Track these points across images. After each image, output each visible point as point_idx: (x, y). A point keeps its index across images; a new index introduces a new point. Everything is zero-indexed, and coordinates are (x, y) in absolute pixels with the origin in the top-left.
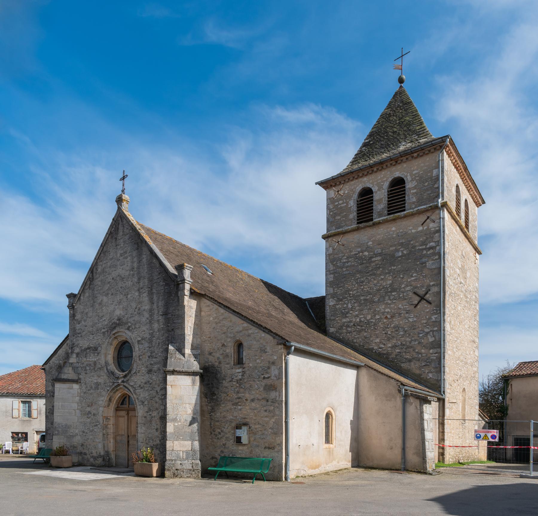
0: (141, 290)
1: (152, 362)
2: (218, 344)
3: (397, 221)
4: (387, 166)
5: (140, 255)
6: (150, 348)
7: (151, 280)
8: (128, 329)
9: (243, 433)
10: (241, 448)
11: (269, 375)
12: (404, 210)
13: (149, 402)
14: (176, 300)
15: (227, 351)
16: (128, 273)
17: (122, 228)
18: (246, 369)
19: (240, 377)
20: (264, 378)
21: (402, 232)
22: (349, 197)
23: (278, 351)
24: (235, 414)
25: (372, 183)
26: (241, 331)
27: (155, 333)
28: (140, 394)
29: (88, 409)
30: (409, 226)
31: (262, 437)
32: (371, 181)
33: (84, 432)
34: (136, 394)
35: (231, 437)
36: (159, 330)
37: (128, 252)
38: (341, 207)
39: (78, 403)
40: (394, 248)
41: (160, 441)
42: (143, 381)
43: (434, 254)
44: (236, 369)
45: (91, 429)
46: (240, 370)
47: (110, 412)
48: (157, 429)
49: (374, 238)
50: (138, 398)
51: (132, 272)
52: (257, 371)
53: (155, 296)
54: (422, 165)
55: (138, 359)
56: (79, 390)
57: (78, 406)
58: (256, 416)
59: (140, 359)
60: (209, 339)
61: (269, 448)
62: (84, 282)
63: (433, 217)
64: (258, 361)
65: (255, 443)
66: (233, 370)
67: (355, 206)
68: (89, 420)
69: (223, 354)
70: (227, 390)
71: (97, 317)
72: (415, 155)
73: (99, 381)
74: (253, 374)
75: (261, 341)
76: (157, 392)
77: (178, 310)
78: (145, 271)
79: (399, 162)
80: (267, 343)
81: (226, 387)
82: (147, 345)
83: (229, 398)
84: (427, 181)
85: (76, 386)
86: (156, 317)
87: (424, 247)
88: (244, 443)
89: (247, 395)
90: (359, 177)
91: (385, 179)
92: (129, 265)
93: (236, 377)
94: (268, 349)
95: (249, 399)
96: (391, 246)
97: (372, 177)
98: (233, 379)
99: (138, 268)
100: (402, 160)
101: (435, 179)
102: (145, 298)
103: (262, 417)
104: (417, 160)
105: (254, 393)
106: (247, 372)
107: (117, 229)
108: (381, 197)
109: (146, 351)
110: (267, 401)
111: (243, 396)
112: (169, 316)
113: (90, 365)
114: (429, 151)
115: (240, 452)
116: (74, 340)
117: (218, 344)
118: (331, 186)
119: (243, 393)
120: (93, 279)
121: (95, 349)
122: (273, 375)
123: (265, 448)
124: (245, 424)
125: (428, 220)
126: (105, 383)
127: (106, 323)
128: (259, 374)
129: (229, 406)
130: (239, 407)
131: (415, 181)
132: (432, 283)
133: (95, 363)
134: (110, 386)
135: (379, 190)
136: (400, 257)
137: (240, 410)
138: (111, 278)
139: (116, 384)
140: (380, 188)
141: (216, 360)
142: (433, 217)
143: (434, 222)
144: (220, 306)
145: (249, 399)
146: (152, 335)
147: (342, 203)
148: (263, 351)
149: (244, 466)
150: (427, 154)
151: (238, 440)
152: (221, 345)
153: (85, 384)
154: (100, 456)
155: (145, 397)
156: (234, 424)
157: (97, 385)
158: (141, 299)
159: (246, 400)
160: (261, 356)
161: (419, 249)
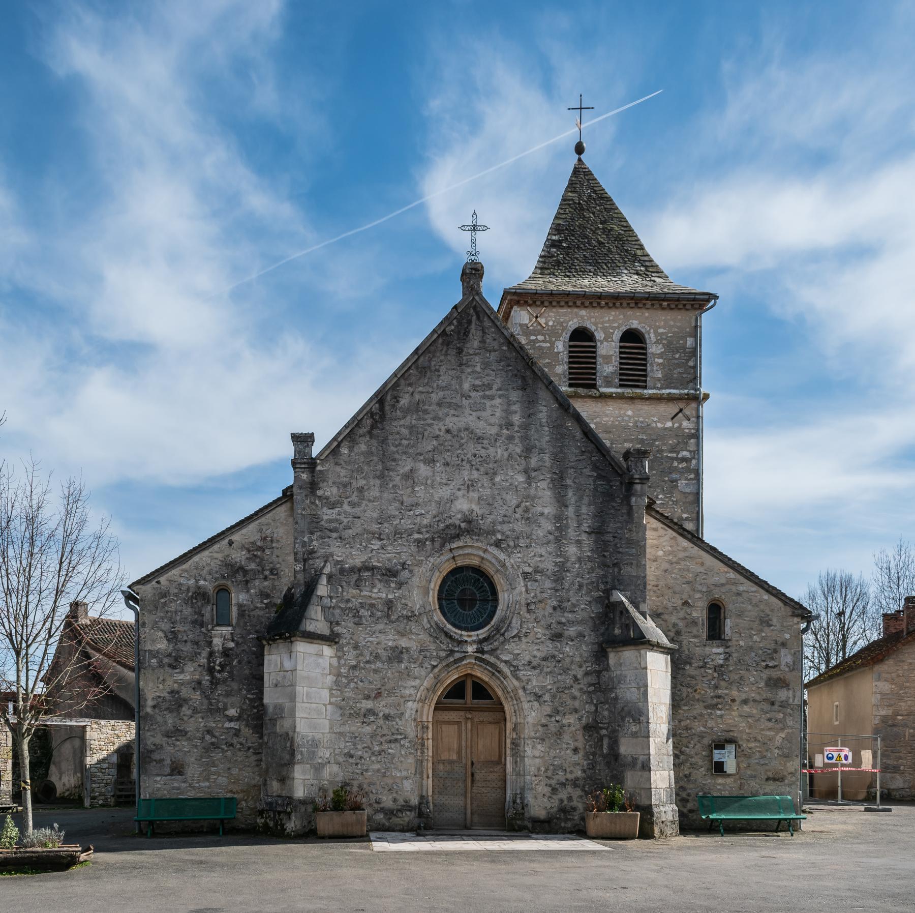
0: (533, 474)
1: (564, 620)
2: (673, 601)
3: (636, 401)
4: (621, 304)
5: (530, 403)
6: (557, 590)
7: (559, 458)
8: (497, 544)
9: (728, 758)
10: (720, 781)
12: (645, 387)
13: (554, 697)
14: (624, 511)
15: (695, 614)
16: (494, 430)
17: (480, 333)
18: (733, 649)
19: (721, 662)
20: (767, 666)
21: (642, 422)
22: (553, 334)
23: (792, 626)
24: (710, 723)
25: (595, 324)
26: (723, 585)
27: (569, 564)
28: (529, 680)
29: (369, 704)
30: (653, 416)
31: (762, 762)
32: (593, 320)
33: (352, 756)
34: (518, 678)
35: (700, 763)
36: (580, 560)
37: (495, 387)
38: (541, 348)
39: (331, 689)
41: (584, 771)
42: (538, 654)
43: (688, 470)
44: (713, 647)
45: (377, 748)
46: (721, 650)
47: (428, 714)
48: (576, 750)
49: (598, 420)
50: (524, 688)
51: (505, 431)
52: (753, 654)
53: (570, 494)
54: (672, 323)
55: (524, 609)
56: (335, 661)
57: (331, 695)
58: (750, 727)
59: (529, 611)
60: (655, 588)
61: (775, 780)
62: (354, 417)
63: (687, 412)
65: (749, 772)
66: (707, 649)
68: (368, 729)
69: (686, 618)
70: (694, 682)
71: (397, 504)
72: (665, 304)
73: (403, 643)
74: (747, 658)
75: (762, 607)
76: (576, 679)
77: (630, 530)
78: (544, 437)
79: (640, 305)
80: (772, 610)
81: (692, 677)
82: (548, 584)
83: (697, 697)
84: (678, 352)
85: (328, 651)
86: (572, 533)
87: (675, 455)
88: (729, 772)
89: (735, 693)
90: (575, 305)
91: (616, 325)
92: (498, 414)
93: (713, 660)
94: (775, 621)
95: (738, 700)
96: (626, 441)
97: (597, 313)
98: (706, 663)
99: (525, 427)
100: (644, 304)
101: (690, 352)
102: (543, 490)
103: (763, 730)
104: (665, 312)
105: (747, 689)
106: (734, 655)
107: (463, 333)
108: (608, 350)
109: (545, 595)
110: (773, 704)
111: (727, 694)
112: (609, 537)
113: (372, 606)
114: (685, 305)
115: (719, 787)
116: (315, 543)
117: (673, 601)
118: (526, 302)
119: (726, 688)
120: (383, 417)
121: (390, 574)
122: (783, 663)
123: (767, 779)
124: (731, 741)
125: (680, 415)
126: (421, 651)
127: (425, 522)
128: (757, 659)
129: (698, 709)
130: (719, 712)
131: (661, 346)
132: (685, 516)
133: (389, 604)
134: (441, 659)
135: (606, 339)
137: (721, 716)
138: (443, 429)
139: (457, 655)
141: (670, 627)
143: (689, 420)
144: (681, 535)
145: (738, 700)
146: (562, 567)
147: (543, 341)
148: (765, 622)
149: (741, 811)
150: (680, 309)
151: (719, 768)
152: (680, 602)
153: (356, 647)
154: (407, 807)
155: (543, 687)
156: (706, 741)
157: (397, 655)
158: (532, 492)
159: (733, 700)
160: (762, 631)
161: (667, 456)
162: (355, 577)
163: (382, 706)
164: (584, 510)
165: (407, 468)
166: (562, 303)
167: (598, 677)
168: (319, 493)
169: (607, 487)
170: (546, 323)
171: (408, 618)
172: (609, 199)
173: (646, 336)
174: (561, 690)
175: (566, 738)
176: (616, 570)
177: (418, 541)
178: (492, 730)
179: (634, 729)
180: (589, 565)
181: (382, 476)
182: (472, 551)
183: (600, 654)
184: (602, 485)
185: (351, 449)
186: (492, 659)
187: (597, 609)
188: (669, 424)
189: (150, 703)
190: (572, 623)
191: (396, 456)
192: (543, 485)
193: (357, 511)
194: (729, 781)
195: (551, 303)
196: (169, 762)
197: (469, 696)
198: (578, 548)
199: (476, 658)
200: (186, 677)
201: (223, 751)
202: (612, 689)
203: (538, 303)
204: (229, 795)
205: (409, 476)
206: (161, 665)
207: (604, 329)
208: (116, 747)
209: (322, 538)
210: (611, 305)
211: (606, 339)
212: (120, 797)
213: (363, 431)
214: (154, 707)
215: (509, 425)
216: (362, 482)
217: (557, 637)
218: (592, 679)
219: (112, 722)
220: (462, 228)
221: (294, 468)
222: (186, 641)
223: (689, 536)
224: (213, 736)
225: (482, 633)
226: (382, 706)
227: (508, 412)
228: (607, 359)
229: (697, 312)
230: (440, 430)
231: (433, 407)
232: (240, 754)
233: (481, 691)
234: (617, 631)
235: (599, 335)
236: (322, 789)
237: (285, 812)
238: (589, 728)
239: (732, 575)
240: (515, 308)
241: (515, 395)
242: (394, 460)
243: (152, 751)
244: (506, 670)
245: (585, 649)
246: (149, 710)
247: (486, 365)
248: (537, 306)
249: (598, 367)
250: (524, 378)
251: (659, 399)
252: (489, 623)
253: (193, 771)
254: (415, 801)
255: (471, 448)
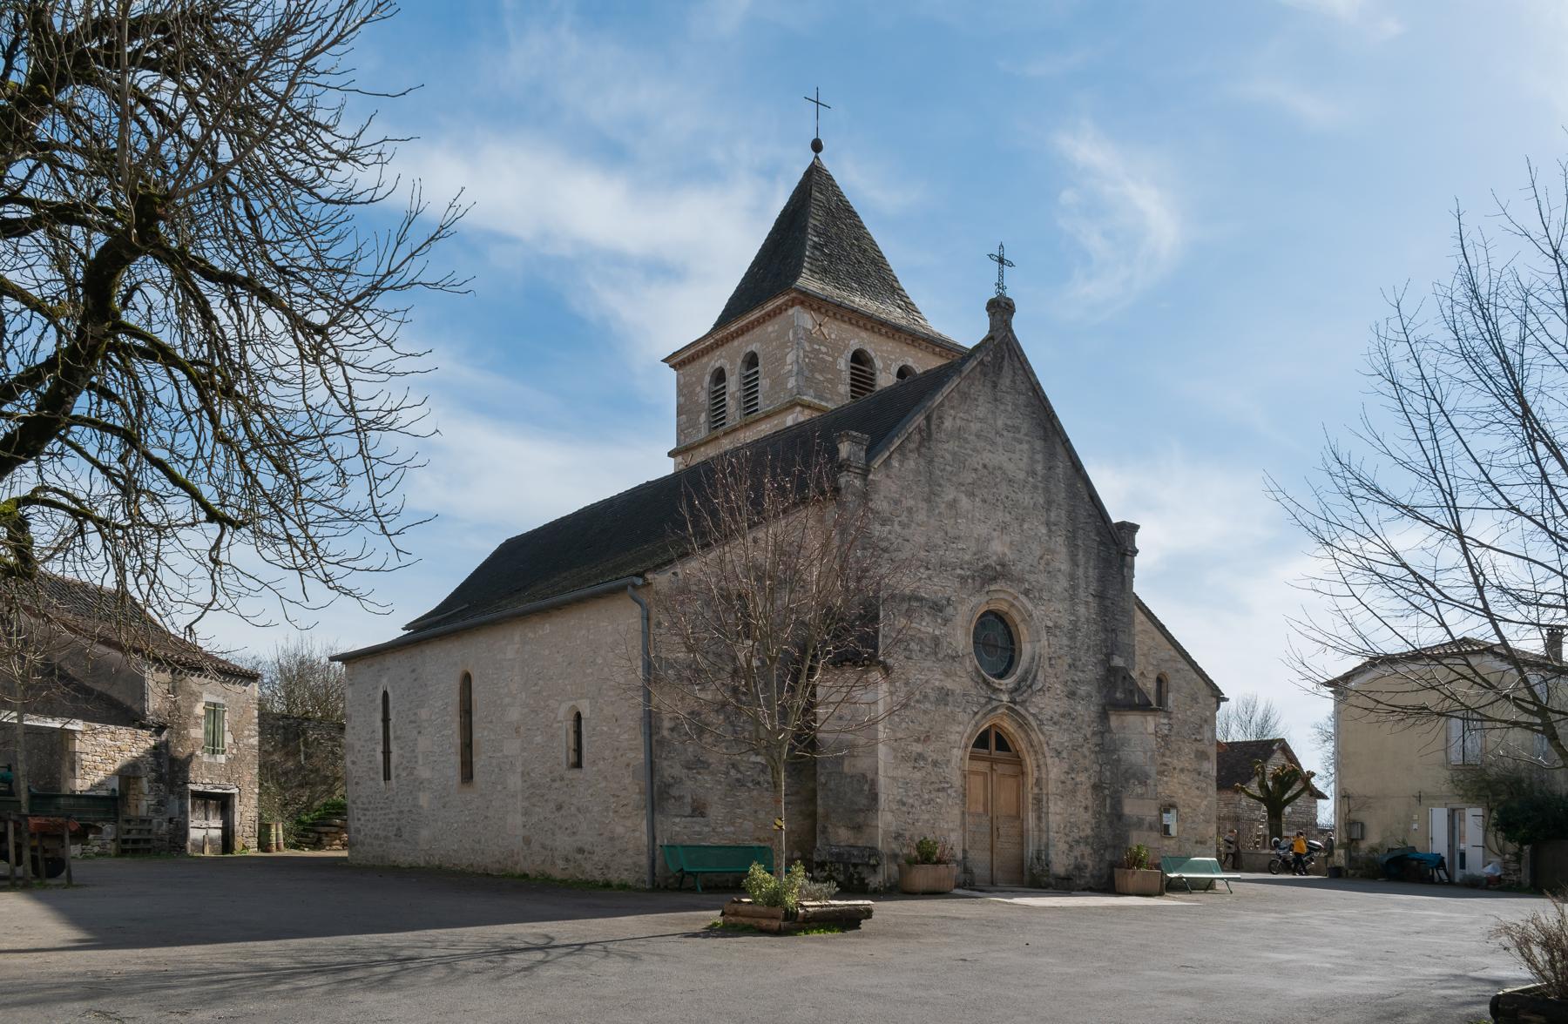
7: (1072, 516)
8: (1026, 593)
9: (1170, 819)
10: (1166, 842)
29: (917, 748)
37: (1023, 431)
38: (824, 361)
48: (1086, 808)
59: (1051, 665)
68: (918, 775)
73: (949, 684)
76: (1086, 739)
86: (1081, 593)
97: (876, 339)
102: (1060, 544)
112: (1108, 603)
113: (921, 640)
121: (937, 608)
127: (967, 558)
133: (936, 640)
139: (995, 704)
146: (1074, 623)
148: (1195, 699)
157: (944, 696)
162: (905, 606)
163: (929, 750)
164: (1091, 572)
165: (951, 497)
171: (953, 658)
172: (855, 215)
174: (1075, 748)
175: (1079, 796)
177: (961, 577)
178: (1011, 782)
179: (1139, 790)
180: (1094, 627)
181: (928, 500)
182: (1001, 597)
183: (1103, 716)
185: (901, 462)
186: (1022, 711)
187: (1100, 671)
189: (667, 724)
190: (1082, 682)
192: (1060, 540)
193: (906, 532)
194: (1172, 842)
197: (992, 744)
198: (1086, 610)
199: (1009, 708)
200: (708, 696)
201: (750, 790)
202: (1115, 751)
204: (755, 844)
205: (953, 505)
206: (679, 677)
208: (117, 765)
212: (125, 841)
213: (912, 446)
214: (672, 730)
215: (1034, 473)
216: (911, 503)
217: (1072, 695)
218: (1097, 739)
219: (112, 728)
224: (739, 771)
226: (929, 750)
227: (1033, 461)
231: (972, 438)
232: (767, 794)
233: (1002, 744)
234: (1119, 695)
235: (879, 364)
237: (867, 864)
238: (1097, 788)
239: (1173, 652)
241: (1039, 444)
243: (670, 786)
244: (1034, 723)
246: (666, 733)
247: (1016, 407)
250: (1045, 429)
253: (716, 812)
255: (1004, 489)
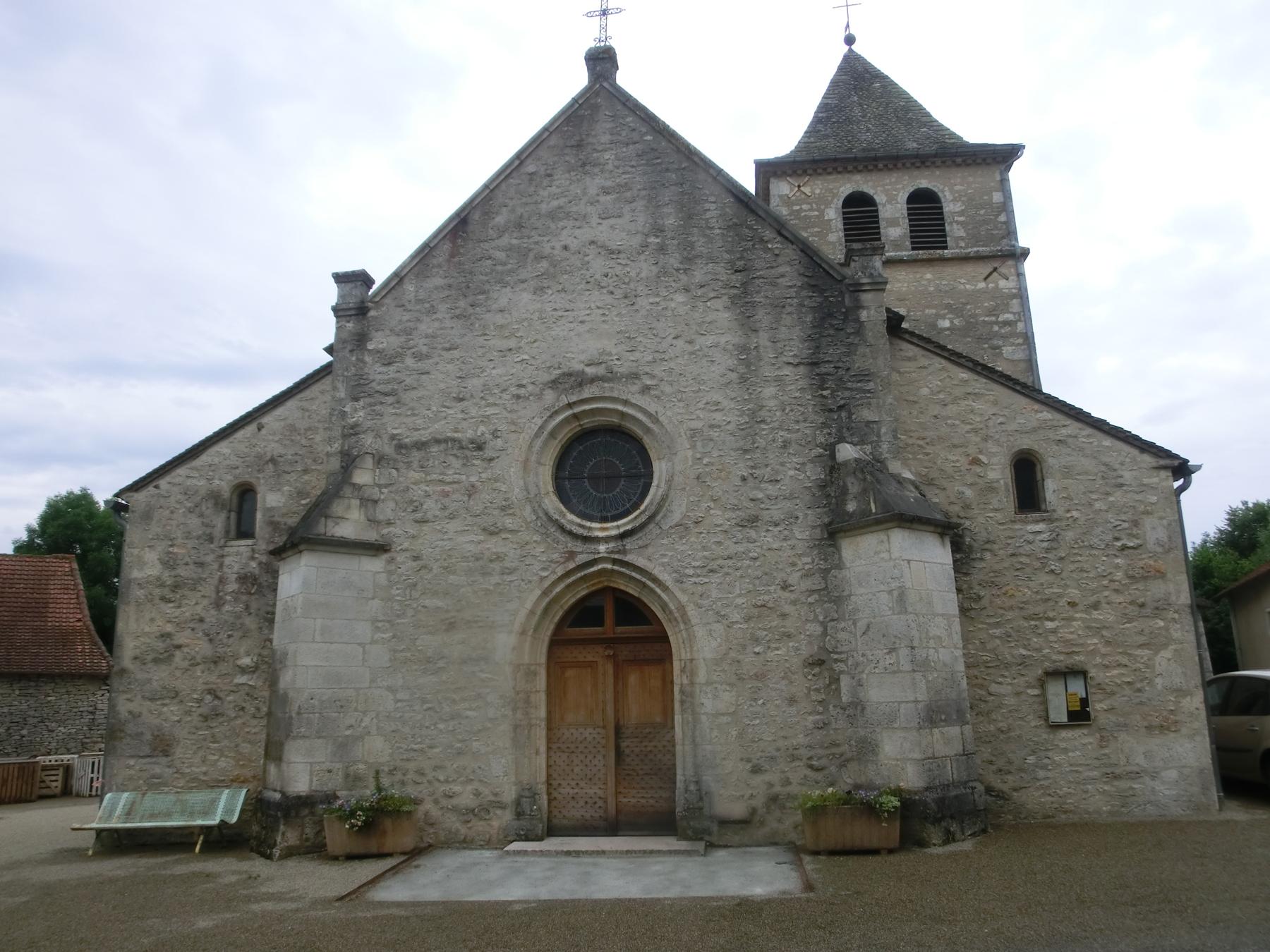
1: (760, 495)
11: (1139, 542)
12: (946, 248)
40: (934, 311)
51: (652, 240)
64: (1097, 505)
67: (840, 219)
85: (374, 565)
96: (928, 307)
111: (1060, 596)
125: (995, 274)
135: (889, 201)
136: (948, 329)
137: (1054, 631)
138: (558, 246)
140: (891, 199)
142: (1003, 270)
166: (830, 170)
167: (824, 578)
168: (370, 346)
169: (819, 300)
170: (813, 193)
173: (940, 195)
176: (844, 414)
184: (811, 297)
187: (815, 473)
188: (982, 285)
191: (487, 287)
195: (815, 170)
196: (148, 737)
203: (800, 172)
207: (886, 192)
209: (371, 405)
210: (890, 166)
211: (889, 201)
215: (658, 230)
220: (589, 14)
221: (337, 316)
222: (187, 564)
223: (970, 365)
225: (625, 524)
228: (893, 223)
229: (1003, 167)
230: (553, 248)
234: (851, 507)
235: (880, 198)
236: (353, 780)
240: (772, 180)
242: (483, 292)
245: (802, 533)
248: (800, 175)
249: (882, 231)
251: (965, 259)
252: (637, 508)
254: (509, 795)
